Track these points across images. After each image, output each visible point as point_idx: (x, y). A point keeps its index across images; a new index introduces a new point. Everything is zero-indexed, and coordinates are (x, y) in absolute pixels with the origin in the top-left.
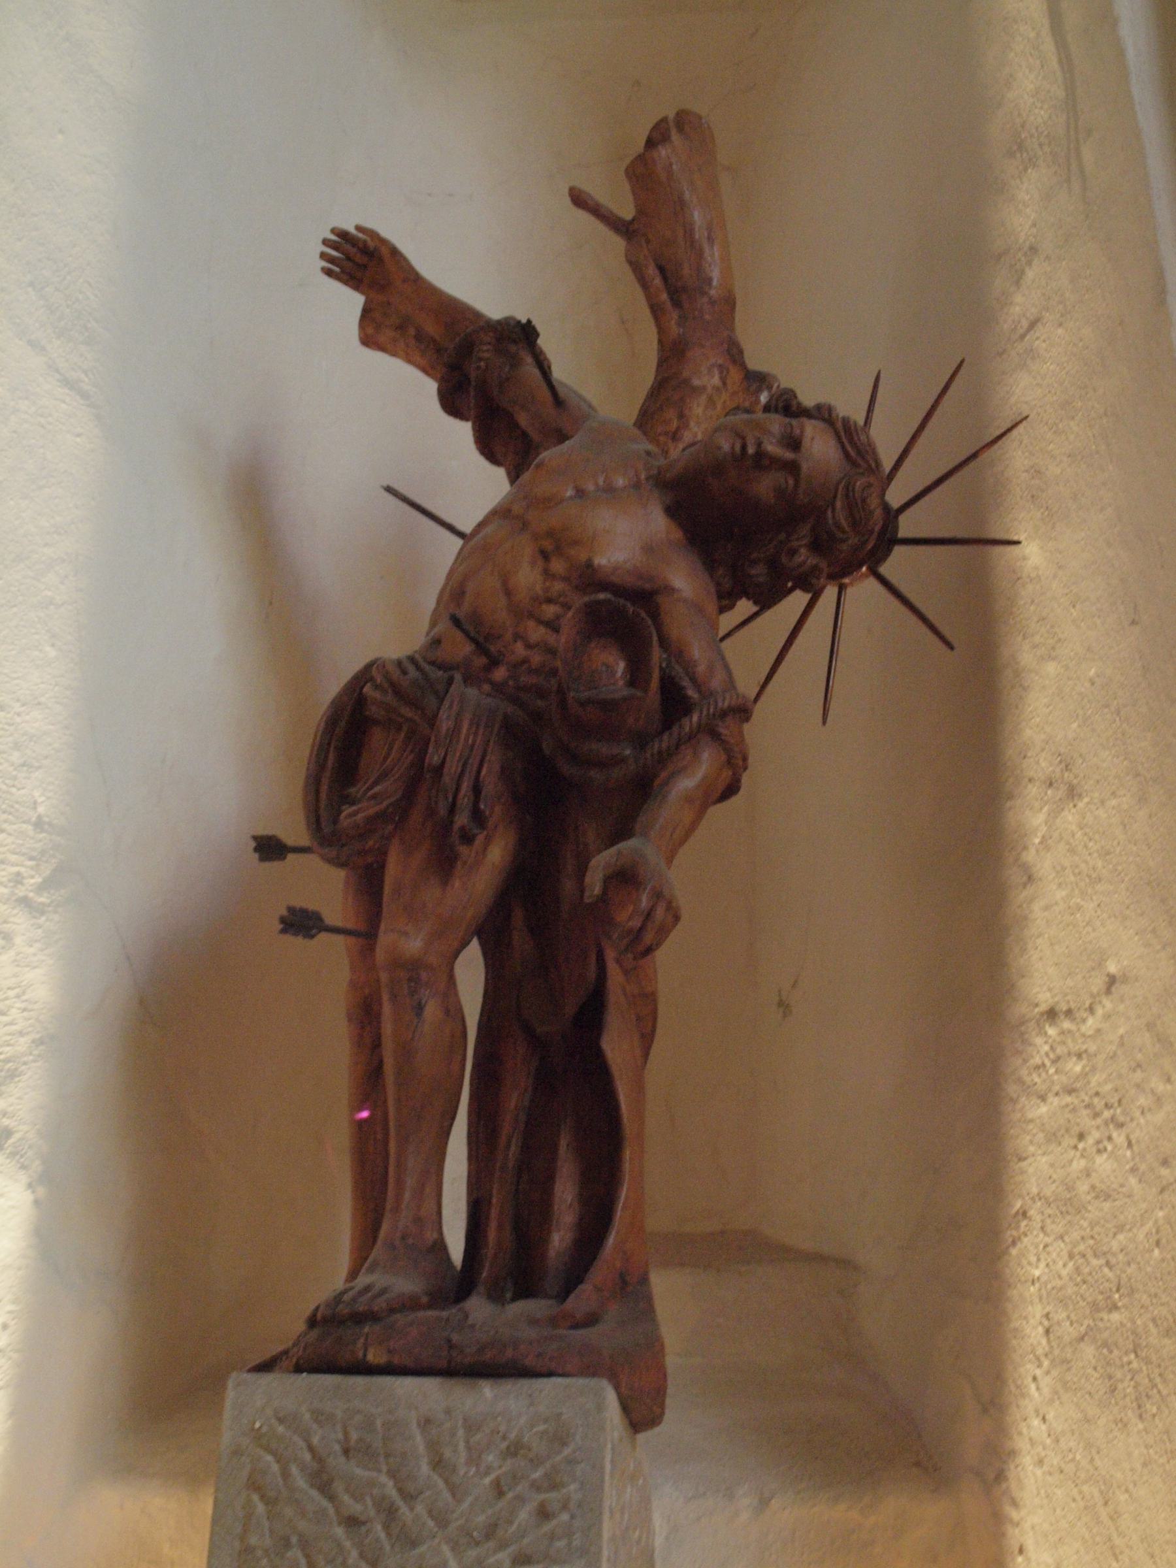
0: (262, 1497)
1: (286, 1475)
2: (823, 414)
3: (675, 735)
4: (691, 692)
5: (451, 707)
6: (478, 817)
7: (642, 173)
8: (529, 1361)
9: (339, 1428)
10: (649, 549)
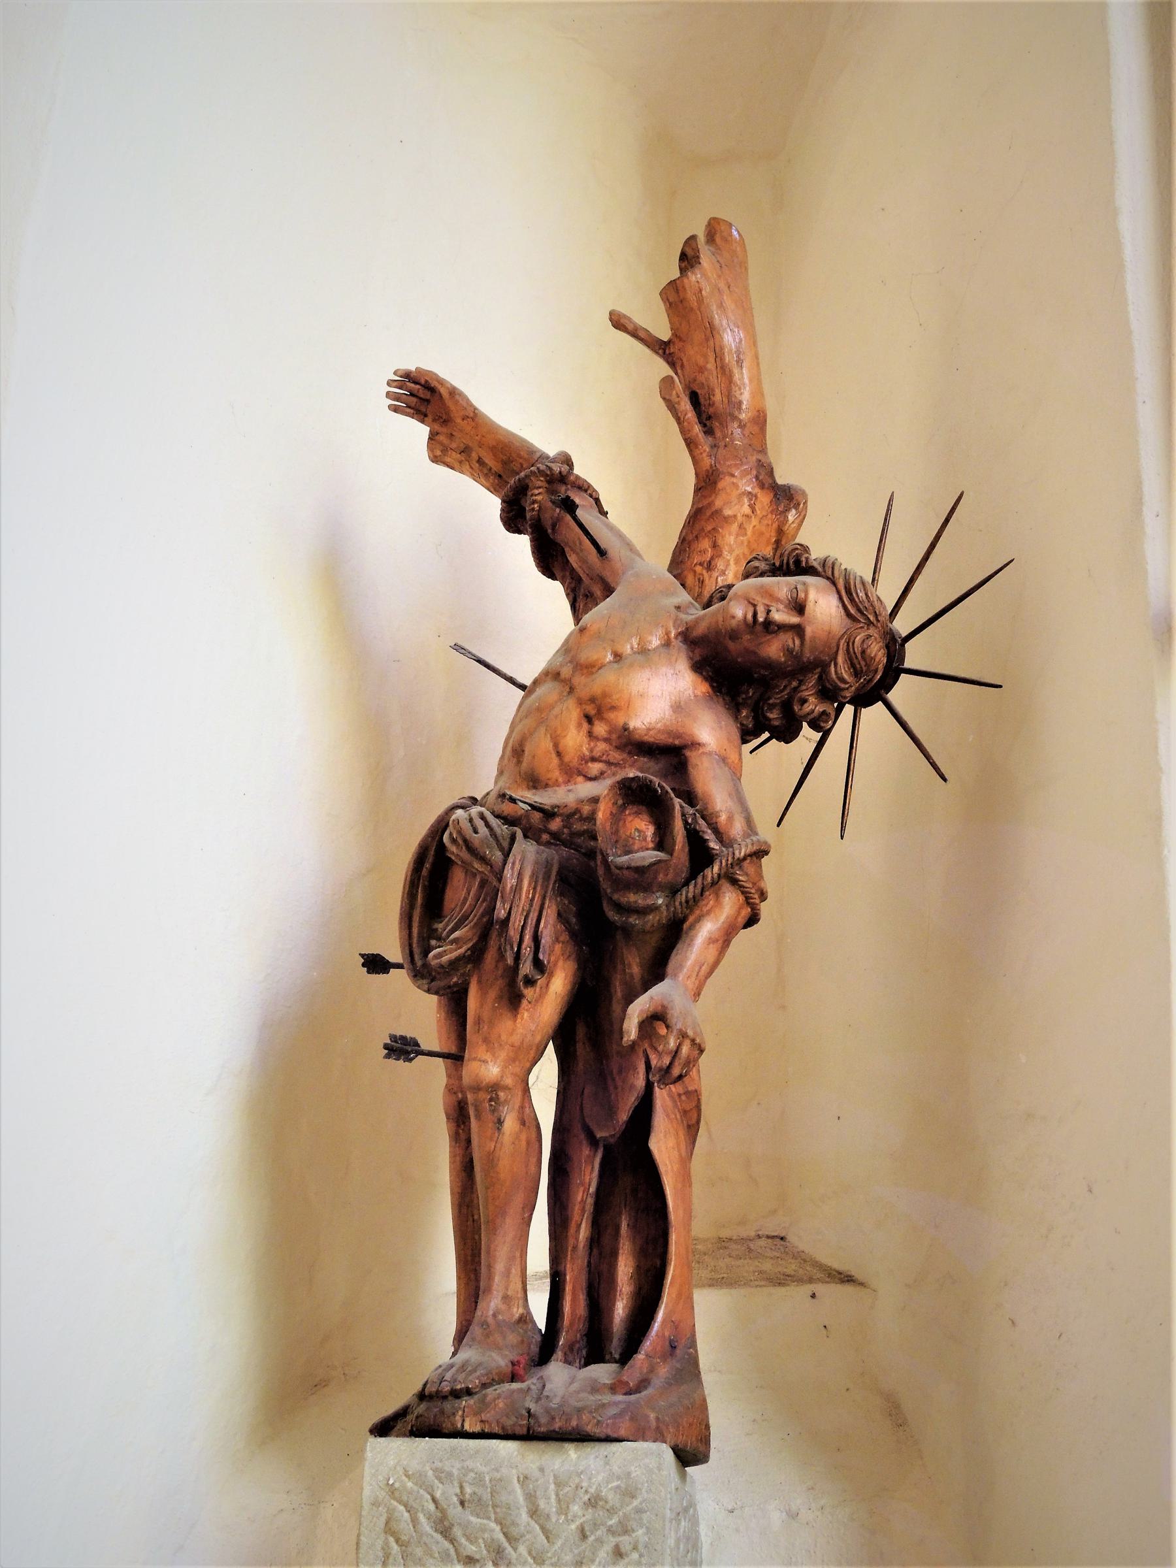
0: (397, 1541)
1: (415, 1521)
2: (825, 571)
3: (699, 886)
4: (714, 845)
5: (513, 864)
6: (538, 965)
7: (675, 298)
8: (590, 1429)
9: (456, 1484)
10: (677, 707)
